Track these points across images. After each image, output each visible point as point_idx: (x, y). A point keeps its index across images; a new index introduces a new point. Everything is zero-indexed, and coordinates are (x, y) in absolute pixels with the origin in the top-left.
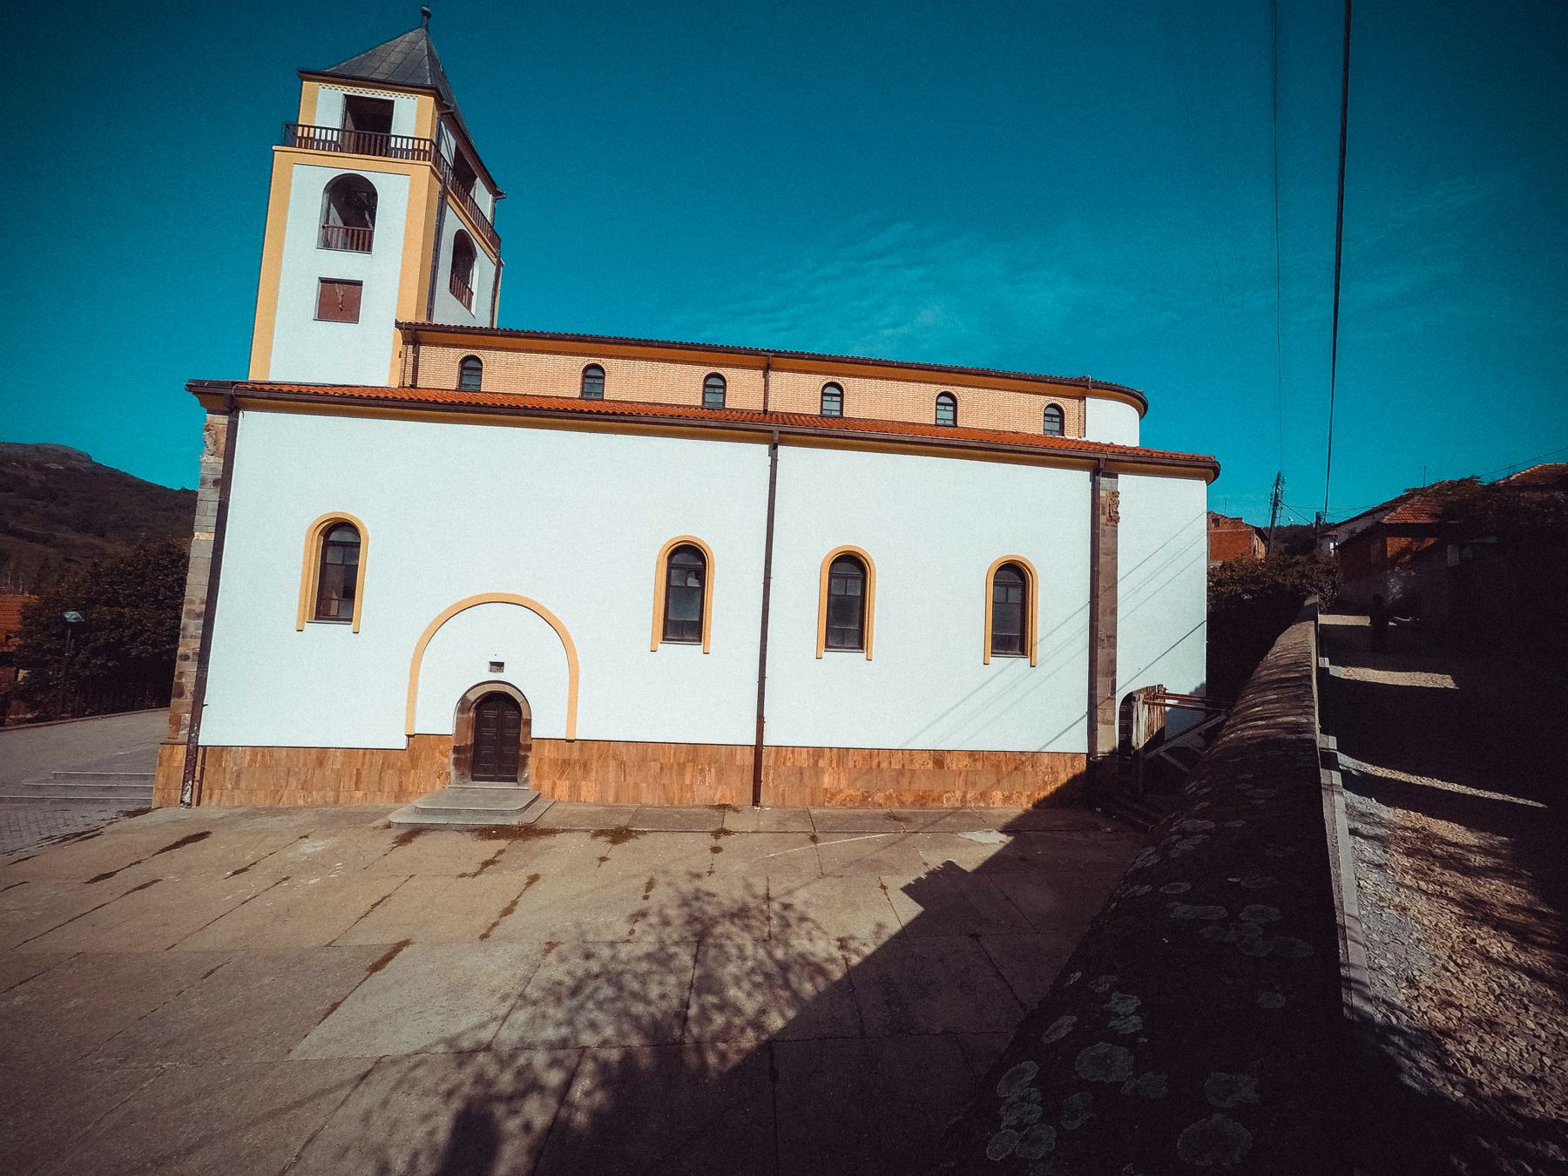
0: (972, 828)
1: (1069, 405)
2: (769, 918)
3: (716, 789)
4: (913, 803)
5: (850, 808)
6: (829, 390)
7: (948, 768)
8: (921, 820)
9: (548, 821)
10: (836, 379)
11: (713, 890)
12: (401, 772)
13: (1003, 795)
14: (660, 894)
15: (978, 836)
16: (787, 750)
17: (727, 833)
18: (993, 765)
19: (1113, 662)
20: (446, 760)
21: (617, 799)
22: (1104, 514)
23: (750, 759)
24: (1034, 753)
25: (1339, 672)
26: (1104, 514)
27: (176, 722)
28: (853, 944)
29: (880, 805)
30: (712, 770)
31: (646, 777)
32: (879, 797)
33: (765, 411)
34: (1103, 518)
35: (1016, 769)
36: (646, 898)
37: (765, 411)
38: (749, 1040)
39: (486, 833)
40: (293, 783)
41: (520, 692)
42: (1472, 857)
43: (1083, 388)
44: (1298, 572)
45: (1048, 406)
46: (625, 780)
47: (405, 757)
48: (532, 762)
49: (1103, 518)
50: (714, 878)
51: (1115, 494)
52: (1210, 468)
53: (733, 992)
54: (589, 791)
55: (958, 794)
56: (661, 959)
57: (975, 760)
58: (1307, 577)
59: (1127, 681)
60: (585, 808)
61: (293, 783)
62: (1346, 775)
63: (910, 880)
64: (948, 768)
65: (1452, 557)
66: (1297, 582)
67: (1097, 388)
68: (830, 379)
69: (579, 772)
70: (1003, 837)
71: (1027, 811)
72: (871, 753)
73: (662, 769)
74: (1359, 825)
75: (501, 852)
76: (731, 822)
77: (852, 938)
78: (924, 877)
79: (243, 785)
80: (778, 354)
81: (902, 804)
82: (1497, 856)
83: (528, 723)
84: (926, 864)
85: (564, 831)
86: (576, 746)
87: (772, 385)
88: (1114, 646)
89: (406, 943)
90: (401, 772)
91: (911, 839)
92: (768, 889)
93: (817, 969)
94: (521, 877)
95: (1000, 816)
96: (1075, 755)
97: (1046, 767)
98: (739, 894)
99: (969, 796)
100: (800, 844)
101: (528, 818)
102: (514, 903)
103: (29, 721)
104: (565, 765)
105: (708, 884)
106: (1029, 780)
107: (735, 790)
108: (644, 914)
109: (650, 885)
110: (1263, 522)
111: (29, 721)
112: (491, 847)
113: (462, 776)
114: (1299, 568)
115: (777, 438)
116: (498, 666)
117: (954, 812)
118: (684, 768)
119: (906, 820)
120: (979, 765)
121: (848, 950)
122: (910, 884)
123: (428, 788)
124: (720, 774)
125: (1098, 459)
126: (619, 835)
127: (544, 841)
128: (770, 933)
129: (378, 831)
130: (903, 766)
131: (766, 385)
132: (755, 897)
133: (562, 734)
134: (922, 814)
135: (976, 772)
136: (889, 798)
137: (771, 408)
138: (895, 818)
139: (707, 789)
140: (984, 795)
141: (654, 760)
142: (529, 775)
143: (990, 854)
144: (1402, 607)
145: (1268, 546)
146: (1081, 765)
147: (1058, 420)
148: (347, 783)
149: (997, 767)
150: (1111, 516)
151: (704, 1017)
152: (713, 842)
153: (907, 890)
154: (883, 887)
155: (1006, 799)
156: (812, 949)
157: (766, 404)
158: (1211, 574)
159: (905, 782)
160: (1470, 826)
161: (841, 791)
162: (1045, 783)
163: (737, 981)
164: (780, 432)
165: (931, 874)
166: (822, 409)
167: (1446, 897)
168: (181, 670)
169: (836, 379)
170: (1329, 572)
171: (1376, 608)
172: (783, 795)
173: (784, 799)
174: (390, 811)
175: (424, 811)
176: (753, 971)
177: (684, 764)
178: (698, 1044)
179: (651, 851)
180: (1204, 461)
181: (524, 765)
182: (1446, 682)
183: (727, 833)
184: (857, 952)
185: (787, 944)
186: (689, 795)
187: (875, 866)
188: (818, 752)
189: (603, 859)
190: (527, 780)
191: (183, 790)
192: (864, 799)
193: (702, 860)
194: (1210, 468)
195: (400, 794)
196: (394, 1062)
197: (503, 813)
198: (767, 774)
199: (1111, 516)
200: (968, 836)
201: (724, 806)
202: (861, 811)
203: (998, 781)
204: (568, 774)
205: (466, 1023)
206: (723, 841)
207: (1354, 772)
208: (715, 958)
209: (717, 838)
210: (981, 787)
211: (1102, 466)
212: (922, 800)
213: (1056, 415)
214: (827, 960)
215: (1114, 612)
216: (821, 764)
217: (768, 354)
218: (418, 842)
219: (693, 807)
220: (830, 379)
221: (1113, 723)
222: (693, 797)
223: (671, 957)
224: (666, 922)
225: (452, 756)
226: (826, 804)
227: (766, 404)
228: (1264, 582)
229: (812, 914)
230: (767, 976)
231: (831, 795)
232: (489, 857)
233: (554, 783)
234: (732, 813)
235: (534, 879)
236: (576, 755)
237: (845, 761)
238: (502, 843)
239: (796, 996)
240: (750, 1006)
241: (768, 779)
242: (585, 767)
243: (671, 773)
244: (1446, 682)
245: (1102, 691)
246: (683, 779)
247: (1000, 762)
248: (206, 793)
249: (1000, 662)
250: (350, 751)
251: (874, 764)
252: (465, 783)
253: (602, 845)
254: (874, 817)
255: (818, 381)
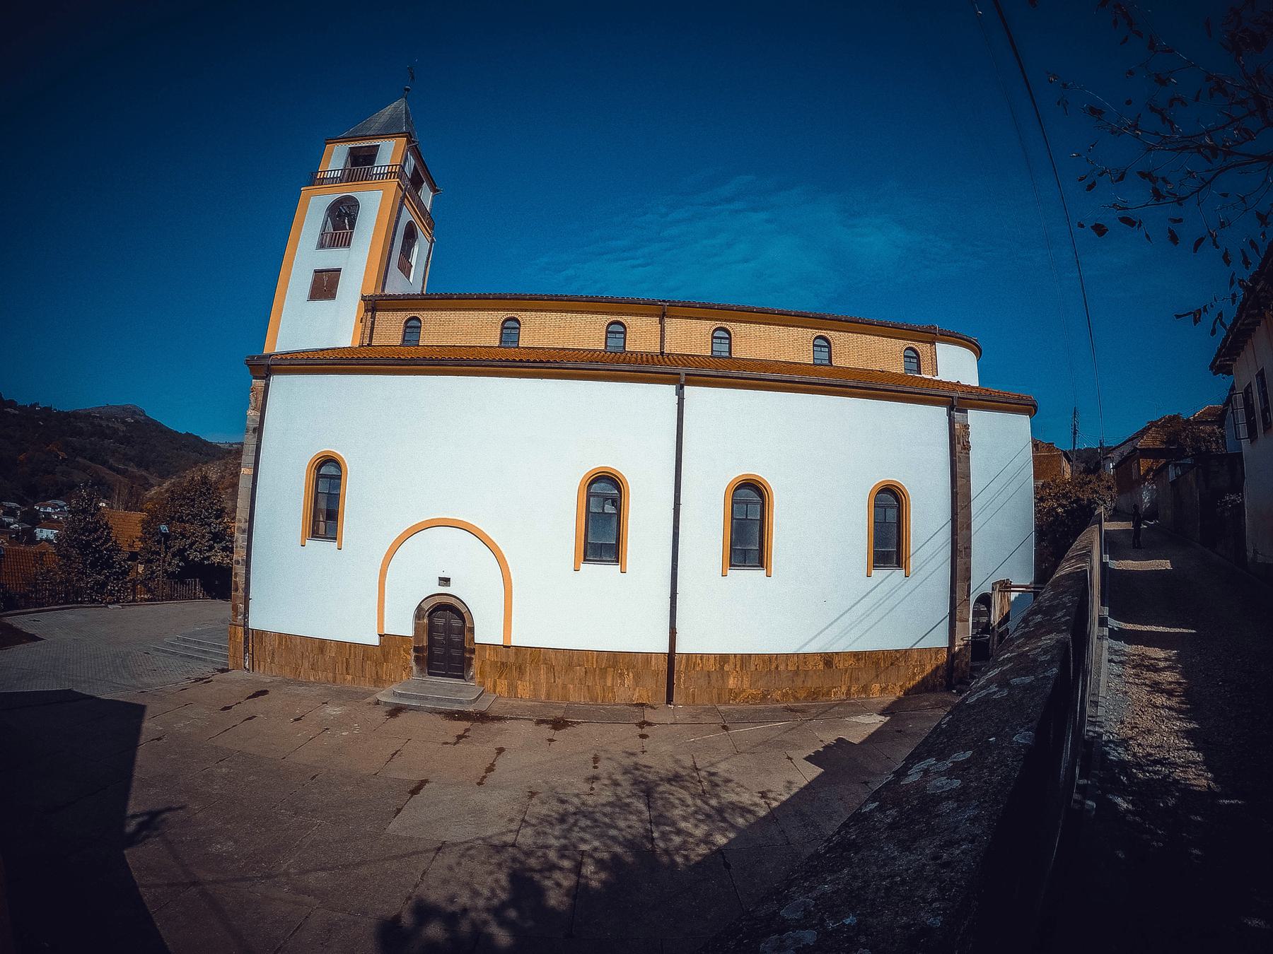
0: (857, 713)
1: (922, 348)
2: (700, 781)
3: (635, 690)
4: (805, 698)
5: (751, 704)
6: (717, 334)
7: (836, 667)
8: (814, 711)
9: (496, 710)
10: (724, 324)
11: (650, 764)
12: (377, 664)
13: (881, 687)
14: (604, 767)
15: (862, 719)
16: (696, 657)
17: (650, 724)
18: (873, 662)
19: (968, 570)
20: (409, 657)
21: (548, 696)
22: (959, 443)
23: (664, 666)
24: (906, 651)
25: (1114, 564)
26: (959, 443)
27: (235, 608)
28: (771, 795)
29: (778, 701)
30: (631, 674)
31: (573, 679)
32: (777, 695)
33: (662, 353)
34: (958, 445)
35: (892, 664)
36: (595, 767)
37: (662, 353)
38: (703, 850)
39: (451, 715)
40: (306, 664)
41: (458, 599)
42: (1160, 663)
43: (932, 336)
44: (1091, 488)
45: (906, 349)
46: (555, 682)
47: (379, 652)
48: (476, 663)
49: (958, 445)
50: (647, 755)
51: (966, 427)
52: (1031, 405)
53: (683, 825)
54: (524, 689)
55: (844, 689)
56: (621, 806)
57: (858, 660)
58: (1097, 492)
59: (980, 582)
60: (522, 703)
61: (306, 664)
62: (1111, 630)
63: (811, 752)
64: (836, 667)
65: (1172, 474)
66: (1091, 497)
67: (944, 335)
68: (719, 324)
69: (515, 674)
70: (881, 718)
71: (899, 697)
72: (768, 659)
73: (586, 672)
74: (1114, 657)
75: (467, 730)
76: (649, 715)
77: (770, 791)
78: (821, 750)
79: (276, 659)
80: (673, 304)
81: (797, 699)
82: (1169, 660)
83: (472, 630)
84: (821, 741)
85: (511, 719)
86: (512, 651)
87: (667, 330)
88: (969, 555)
89: (426, 781)
90: (377, 664)
91: (807, 725)
92: (694, 763)
93: (744, 810)
94: (490, 748)
95: (878, 703)
96: (938, 650)
97: (916, 662)
98: (670, 765)
99: (853, 689)
100: (714, 732)
101: (482, 707)
102: (493, 765)
103: (146, 600)
104: (502, 668)
105: (643, 760)
106: (902, 672)
107: (650, 689)
108: (595, 778)
109: (596, 759)
110: (1069, 448)
111: (146, 600)
112: (461, 726)
113: (422, 670)
114: (1090, 486)
115: (684, 380)
116: (445, 581)
117: (841, 703)
118: (606, 672)
119: (802, 711)
120: (862, 664)
121: (769, 798)
122: (810, 755)
123: (397, 679)
124: (637, 677)
125: (952, 397)
126: (558, 724)
127: (497, 725)
128: (703, 791)
129: (371, 706)
130: (798, 667)
131: (663, 330)
132: (684, 768)
133: (499, 641)
134: (815, 706)
135: (859, 669)
136: (785, 695)
137: (666, 351)
138: (792, 710)
139: (626, 690)
140: (865, 689)
141: (580, 666)
142: (474, 674)
143: (872, 730)
144: (1152, 513)
145: (1072, 466)
146: (944, 657)
147: (915, 361)
148: (340, 668)
149: (877, 663)
150: (964, 445)
151: (664, 836)
152: (639, 731)
153: (809, 759)
154: (790, 759)
155: (883, 690)
156: (740, 799)
157: (662, 346)
158: (1037, 490)
159: (799, 682)
160: (1162, 648)
161: (744, 690)
162: (914, 674)
163: (685, 819)
164: (686, 374)
165: (826, 747)
166: (712, 351)
167: (1145, 684)
168: (237, 571)
169: (724, 324)
170: (1109, 488)
171: (1135, 515)
172: (693, 695)
173: (694, 698)
174: (374, 693)
175: (401, 695)
176: (696, 812)
177: (606, 669)
178: (666, 851)
179: (588, 737)
180: (1027, 400)
181: (470, 665)
182: (1166, 565)
183: (650, 724)
184: (775, 799)
185: (717, 796)
186: (610, 695)
187: (781, 745)
188: (723, 658)
189: (551, 740)
190: (472, 678)
191: (244, 659)
192: (765, 697)
193: (634, 744)
194: (1031, 405)
195: (378, 681)
196: (455, 845)
197: (461, 702)
198: (679, 678)
199: (964, 445)
200: (854, 719)
201: (642, 705)
202: (762, 707)
203: (877, 676)
204: (506, 674)
205: (493, 830)
206: (646, 730)
207: (1115, 629)
208: (664, 806)
209: (642, 728)
210: (862, 683)
211: (955, 403)
212: (814, 695)
213: (913, 357)
214: (752, 805)
215: (969, 527)
216: (726, 668)
217: (664, 304)
218: (403, 717)
219: (614, 705)
220: (719, 324)
221: (968, 621)
222: (614, 697)
223: (628, 805)
224: (616, 784)
225: (413, 654)
226: (731, 702)
227: (662, 346)
228: (1071, 497)
229: (732, 776)
230: (708, 816)
231: (734, 694)
232: (461, 732)
233: (495, 682)
234: (650, 710)
235: (500, 751)
236: (512, 659)
237: (748, 664)
238: (467, 724)
239: (733, 827)
240: (699, 832)
241: (680, 682)
242: (521, 669)
243: (594, 678)
244: (1166, 565)
245: (960, 595)
246: (605, 682)
247: (879, 659)
248: (256, 663)
249: (878, 574)
250: (341, 645)
251: (773, 667)
252: (423, 676)
253: (546, 731)
254: (775, 710)
255: (708, 326)
